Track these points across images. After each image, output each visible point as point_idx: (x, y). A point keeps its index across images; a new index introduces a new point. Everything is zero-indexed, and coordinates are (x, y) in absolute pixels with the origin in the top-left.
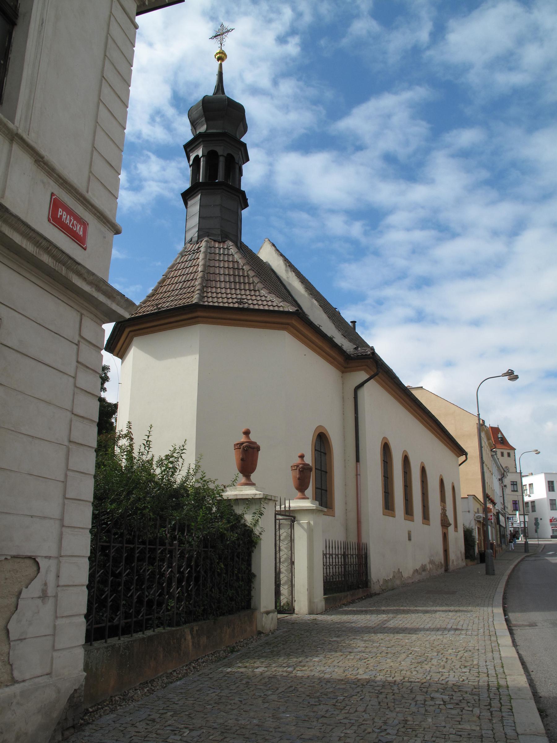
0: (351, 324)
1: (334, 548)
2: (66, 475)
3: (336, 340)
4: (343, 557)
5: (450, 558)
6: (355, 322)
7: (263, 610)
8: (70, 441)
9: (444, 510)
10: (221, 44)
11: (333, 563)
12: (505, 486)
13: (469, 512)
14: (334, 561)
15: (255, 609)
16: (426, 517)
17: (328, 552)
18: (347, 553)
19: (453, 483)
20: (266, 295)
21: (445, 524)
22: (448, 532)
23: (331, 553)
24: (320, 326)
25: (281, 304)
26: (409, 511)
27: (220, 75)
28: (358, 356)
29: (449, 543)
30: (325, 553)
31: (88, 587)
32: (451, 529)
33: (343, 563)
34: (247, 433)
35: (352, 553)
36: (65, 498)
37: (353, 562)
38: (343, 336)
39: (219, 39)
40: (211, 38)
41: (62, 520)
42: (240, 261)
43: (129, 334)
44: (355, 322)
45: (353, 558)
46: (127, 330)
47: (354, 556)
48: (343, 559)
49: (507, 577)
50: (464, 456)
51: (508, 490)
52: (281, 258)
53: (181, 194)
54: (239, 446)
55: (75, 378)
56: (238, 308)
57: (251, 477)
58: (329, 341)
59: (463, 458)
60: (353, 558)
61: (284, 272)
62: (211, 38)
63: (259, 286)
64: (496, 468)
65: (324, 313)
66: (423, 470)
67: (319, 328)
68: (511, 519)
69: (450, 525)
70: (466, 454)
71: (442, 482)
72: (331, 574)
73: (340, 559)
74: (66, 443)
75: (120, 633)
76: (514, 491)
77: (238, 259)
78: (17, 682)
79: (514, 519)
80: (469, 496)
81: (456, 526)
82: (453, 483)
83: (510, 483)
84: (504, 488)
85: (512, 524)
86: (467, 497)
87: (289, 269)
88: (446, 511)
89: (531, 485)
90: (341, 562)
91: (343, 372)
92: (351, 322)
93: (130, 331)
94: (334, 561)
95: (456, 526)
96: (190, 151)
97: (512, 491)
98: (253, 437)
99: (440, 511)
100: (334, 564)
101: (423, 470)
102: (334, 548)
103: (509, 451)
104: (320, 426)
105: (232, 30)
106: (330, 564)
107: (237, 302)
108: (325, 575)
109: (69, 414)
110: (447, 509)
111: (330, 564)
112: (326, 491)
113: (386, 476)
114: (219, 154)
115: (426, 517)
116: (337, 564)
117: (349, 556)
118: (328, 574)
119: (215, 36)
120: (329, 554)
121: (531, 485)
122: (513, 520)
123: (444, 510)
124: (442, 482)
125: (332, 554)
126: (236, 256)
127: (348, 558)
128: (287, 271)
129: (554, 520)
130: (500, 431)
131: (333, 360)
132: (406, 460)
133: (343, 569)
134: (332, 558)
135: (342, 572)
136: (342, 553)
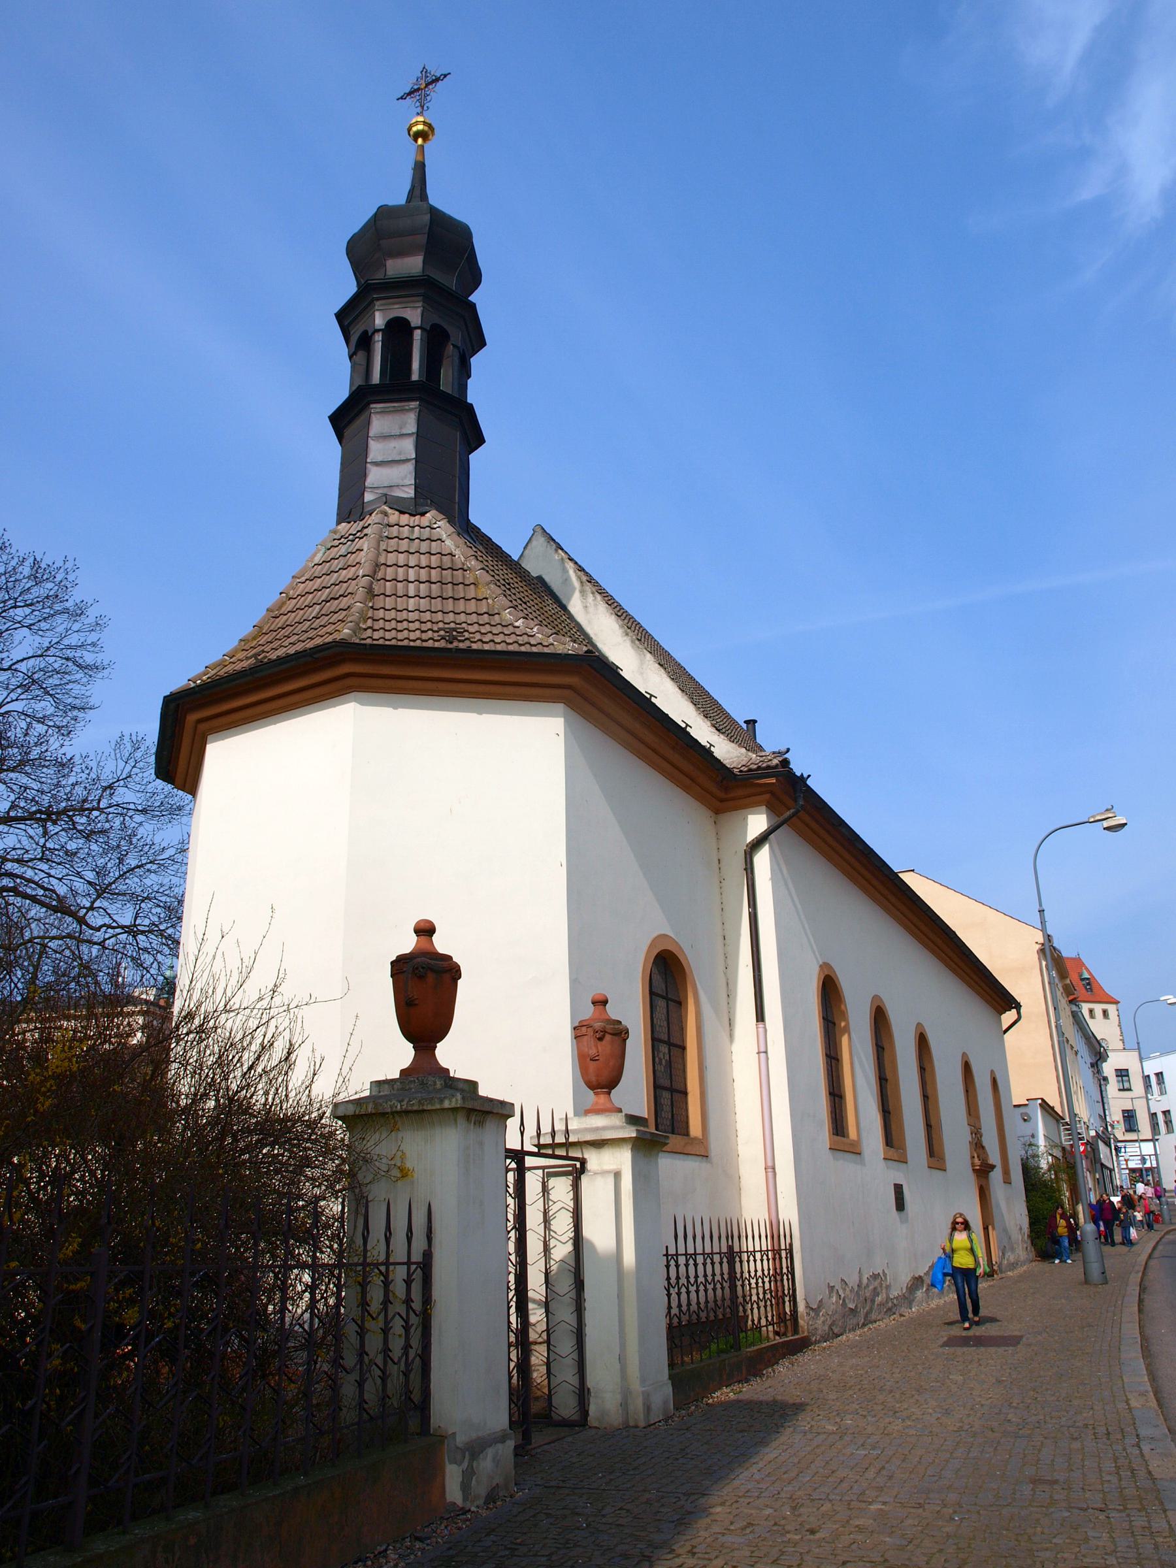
0: (744, 726)
1: (699, 1239)
3: (694, 732)
4: (725, 1260)
6: (755, 722)
9: (976, 1132)
10: (422, 107)
11: (714, 1275)
12: (1105, 1079)
14: (717, 1271)
16: (935, 1154)
17: (681, 1250)
18: (736, 1249)
19: (992, 1072)
21: (983, 1171)
23: (708, 1250)
24: (651, 696)
25: (551, 640)
26: (892, 1137)
27: (420, 169)
28: (750, 770)
29: (872, 1061)
30: (672, 1251)
32: (996, 1176)
33: (726, 1277)
35: (708, 1250)
37: (756, 1271)
38: (714, 730)
39: (418, 98)
40: (402, 98)
42: (457, 552)
44: (755, 722)
45: (755, 1261)
47: (717, 1258)
48: (725, 1266)
49: (576, 1140)
50: (1014, 1011)
51: (1112, 1088)
53: (329, 417)
57: (437, 1052)
58: (679, 735)
59: (1009, 1017)
60: (755, 1261)
62: (402, 98)
64: (1084, 1039)
65: (668, 680)
66: (922, 1042)
67: (649, 700)
68: (1123, 1150)
69: (993, 1167)
70: (1018, 1006)
71: (967, 1068)
72: (711, 1305)
73: (717, 1266)
76: (1124, 1090)
77: (453, 548)
79: (1127, 1150)
80: (1031, 1102)
82: (992, 1072)
83: (1114, 1073)
84: (1102, 1082)
85: (1126, 1161)
86: (1027, 1103)
88: (981, 1136)
89: (1159, 1075)
90: (722, 1274)
91: (717, 812)
92: (745, 722)
94: (717, 1271)
96: (349, 324)
97: (1120, 1090)
98: (442, 944)
99: (966, 1136)
100: (701, 1279)
101: (922, 1042)
102: (699, 1239)
103: (1105, 1006)
104: (663, 937)
105: (445, 76)
106: (706, 1280)
107: (443, 638)
108: (675, 1311)
110: (983, 1131)
111: (763, 1274)
113: (833, 1054)
114: (413, 325)
115: (935, 1154)
116: (710, 1278)
117: (745, 1256)
118: (684, 1308)
119: (409, 94)
120: (686, 1254)
121: (1159, 1075)
123: (976, 1132)
124: (967, 1068)
125: (695, 1254)
126: (448, 542)
127: (741, 1262)
130: (1083, 965)
131: (688, 781)
132: (880, 1018)
133: (727, 1291)
134: (713, 1263)
135: (723, 1299)
136: (724, 1250)
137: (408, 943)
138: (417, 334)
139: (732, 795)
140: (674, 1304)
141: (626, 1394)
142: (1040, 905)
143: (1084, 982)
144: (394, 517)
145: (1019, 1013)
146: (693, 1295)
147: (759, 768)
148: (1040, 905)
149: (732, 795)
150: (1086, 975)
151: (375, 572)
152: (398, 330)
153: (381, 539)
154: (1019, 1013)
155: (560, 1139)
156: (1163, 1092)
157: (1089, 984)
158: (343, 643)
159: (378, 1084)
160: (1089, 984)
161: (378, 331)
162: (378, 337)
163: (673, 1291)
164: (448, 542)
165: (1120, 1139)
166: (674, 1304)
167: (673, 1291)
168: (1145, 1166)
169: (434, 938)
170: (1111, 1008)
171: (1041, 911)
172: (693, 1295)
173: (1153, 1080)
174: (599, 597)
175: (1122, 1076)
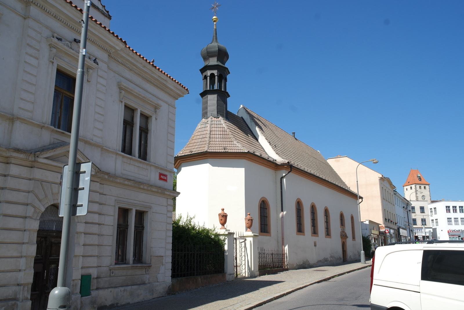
2: (166, 237)
5: (348, 254)
7: (228, 273)
8: (166, 229)
13: (366, 229)
15: (226, 273)
16: (328, 233)
20: (236, 144)
22: (346, 241)
26: (315, 232)
31: (172, 263)
34: (223, 210)
36: (166, 243)
41: (165, 248)
42: (225, 127)
43: (179, 162)
46: (179, 161)
52: (248, 115)
54: (219, 215)
55: (167, 214)
56: (224, 152)
61: (250, 122)
63: (233, 139)
66: (326, 212)
71: (342, 216)
74: (166, 230)
75: (179, 276)
78: (158, 282)
81: (354, 238)
87: (252, 121)
89: (435, 208)
93: (180, 161)
95: (354, 238)
98: (225, 211)
109: (166, 223)
112: (301, 210)
115: (328, 233)
121: (435, 208)
122: (422, 231)
124: (342, 216)
126: (224, 125)
128: (251, 121)
129: (451, 231)
131: (269, 167)
137: (220, 211)
138: (216, 77)
139: (278, 168)
140: (260, 260)
141: (249, 269)
142: (357, 180)
143: (418, 178)
144: (213, 118)
145: (362, 200)
146: (264, 260)
147: (282, 164)
148: (357, 180)
149: (278, 168)
150: (419, 176)
151: (211, 133)
152: (212, 75)
153: (211, 124)
154: (362, 200)
155: (242, 235)
156: (436, 213)
157: (420, 178)
158: (206, 152)
159: (258, 290)
160: (420, 178)
161: (208, 76)
162: (208, 78)
163: (260, 259)
164: (224, 125)
165: (372, 233)
166: (260, 260)
167: (260, 259)
168: (426, 235)
169: (224, 210)
170: (427, 187)
171: (357, 181)
172: (264, 260)
173: (433, 210)
174: (254, 122)
175: (422, 209)
